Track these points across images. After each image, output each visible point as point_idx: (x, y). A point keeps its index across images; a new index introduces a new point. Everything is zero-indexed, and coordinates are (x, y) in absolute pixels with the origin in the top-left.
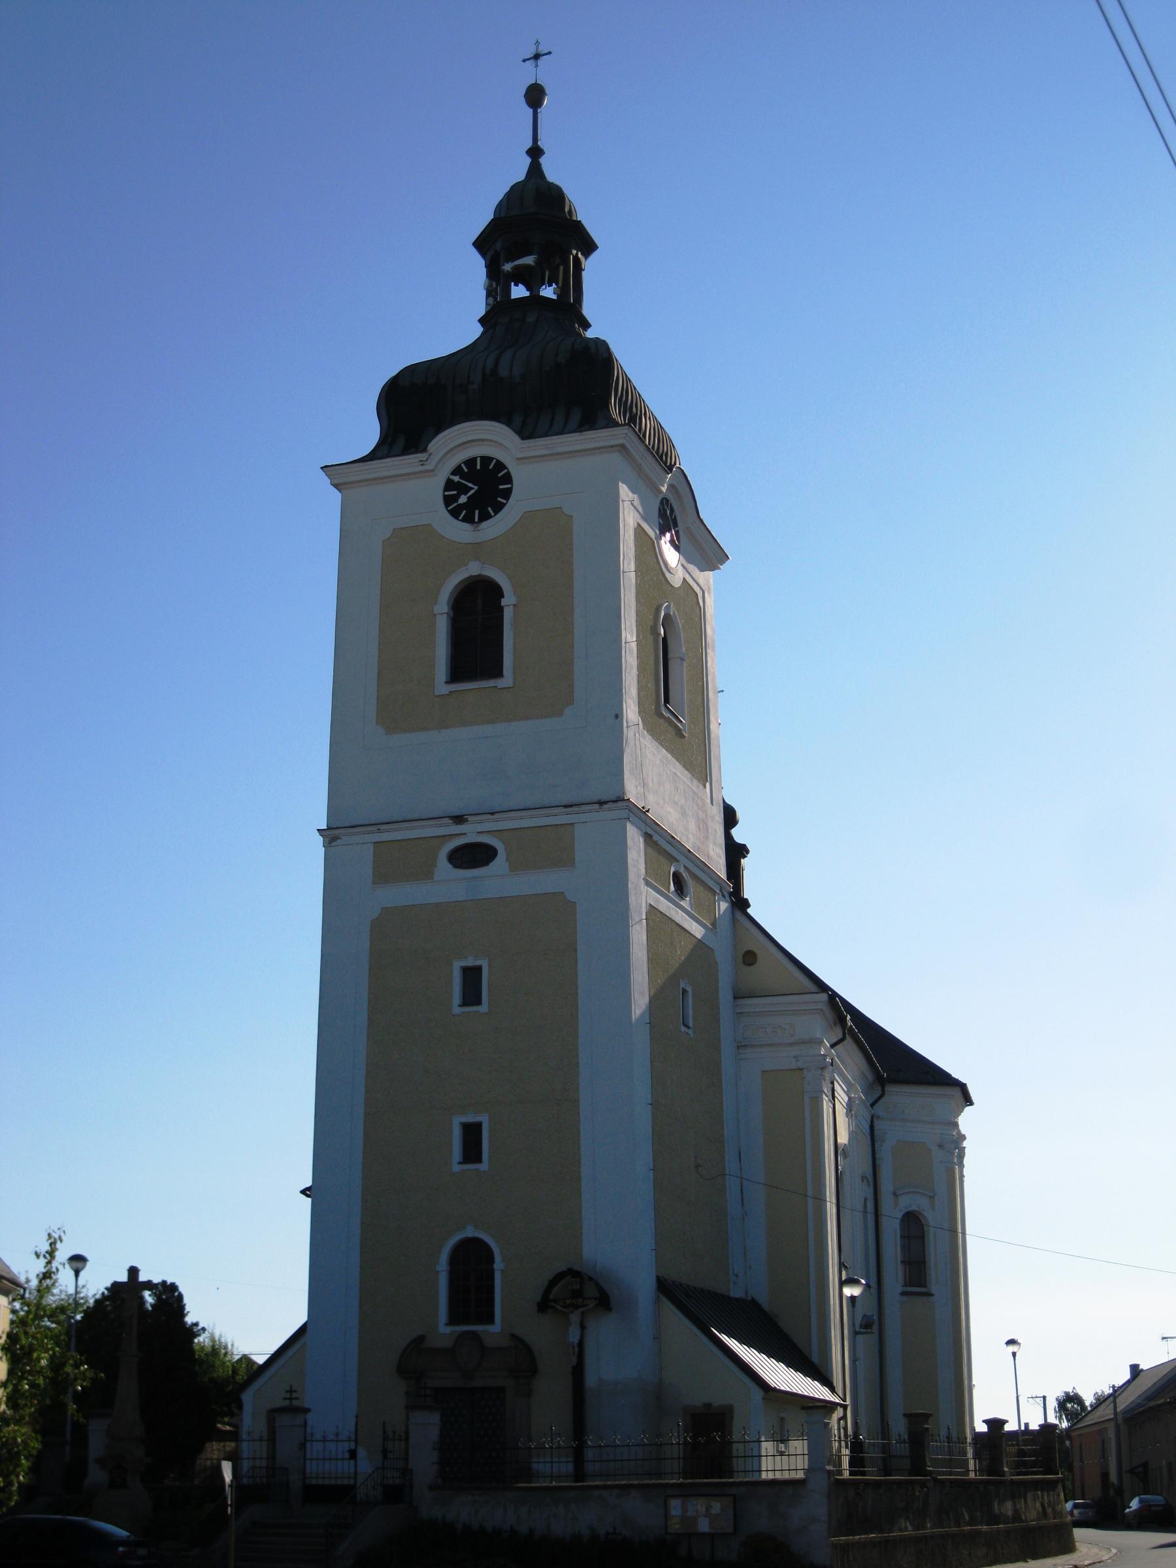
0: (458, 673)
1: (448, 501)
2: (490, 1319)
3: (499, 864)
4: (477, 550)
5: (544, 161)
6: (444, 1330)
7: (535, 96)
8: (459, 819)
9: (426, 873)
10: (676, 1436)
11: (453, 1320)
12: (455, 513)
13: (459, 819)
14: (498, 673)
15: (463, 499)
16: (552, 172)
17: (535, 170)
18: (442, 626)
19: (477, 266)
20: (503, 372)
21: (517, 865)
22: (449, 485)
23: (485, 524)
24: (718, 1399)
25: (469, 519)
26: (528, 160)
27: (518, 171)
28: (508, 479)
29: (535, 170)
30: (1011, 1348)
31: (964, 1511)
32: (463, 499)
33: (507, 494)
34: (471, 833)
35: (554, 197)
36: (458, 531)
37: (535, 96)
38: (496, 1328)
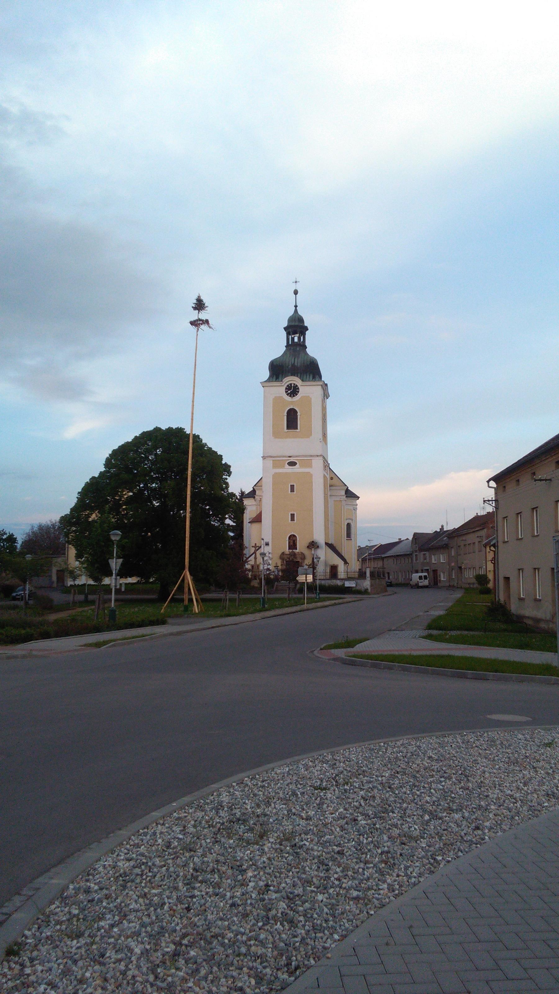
0: (288, 427)
1: (286, 392)
2: (296, 549)
3: (297, 466)
4: (292, 403)
5: (297, 308)
6: (287, 551)
7: (296, 292)
8: (290, 457)
9: (283, 467)
10: (328, 570)
11: (289, 549)
12: (288, 395)
13: (290, 457)
14: (297, 429)
15: (289, 392)
16: (300, 312)
17: (296, 311)
18: (285, 417)
19: (285, 333)
20: (296, 364)
21: (301, 466)
22: (286, 389)
23: (294, 398)
24: (336, 563)
25: (290, 396)
26: (294, 308)
27: (291, 312)
28: (298, 389)
29: (296, 311)
30: (203, 315)
31: (488, 716)
32: (289, 392)
33: (298, 392)
34: (292, 460)
35: (301, 320)
36: (288, 398)
37: (296, 292)
38: (298, 551)
